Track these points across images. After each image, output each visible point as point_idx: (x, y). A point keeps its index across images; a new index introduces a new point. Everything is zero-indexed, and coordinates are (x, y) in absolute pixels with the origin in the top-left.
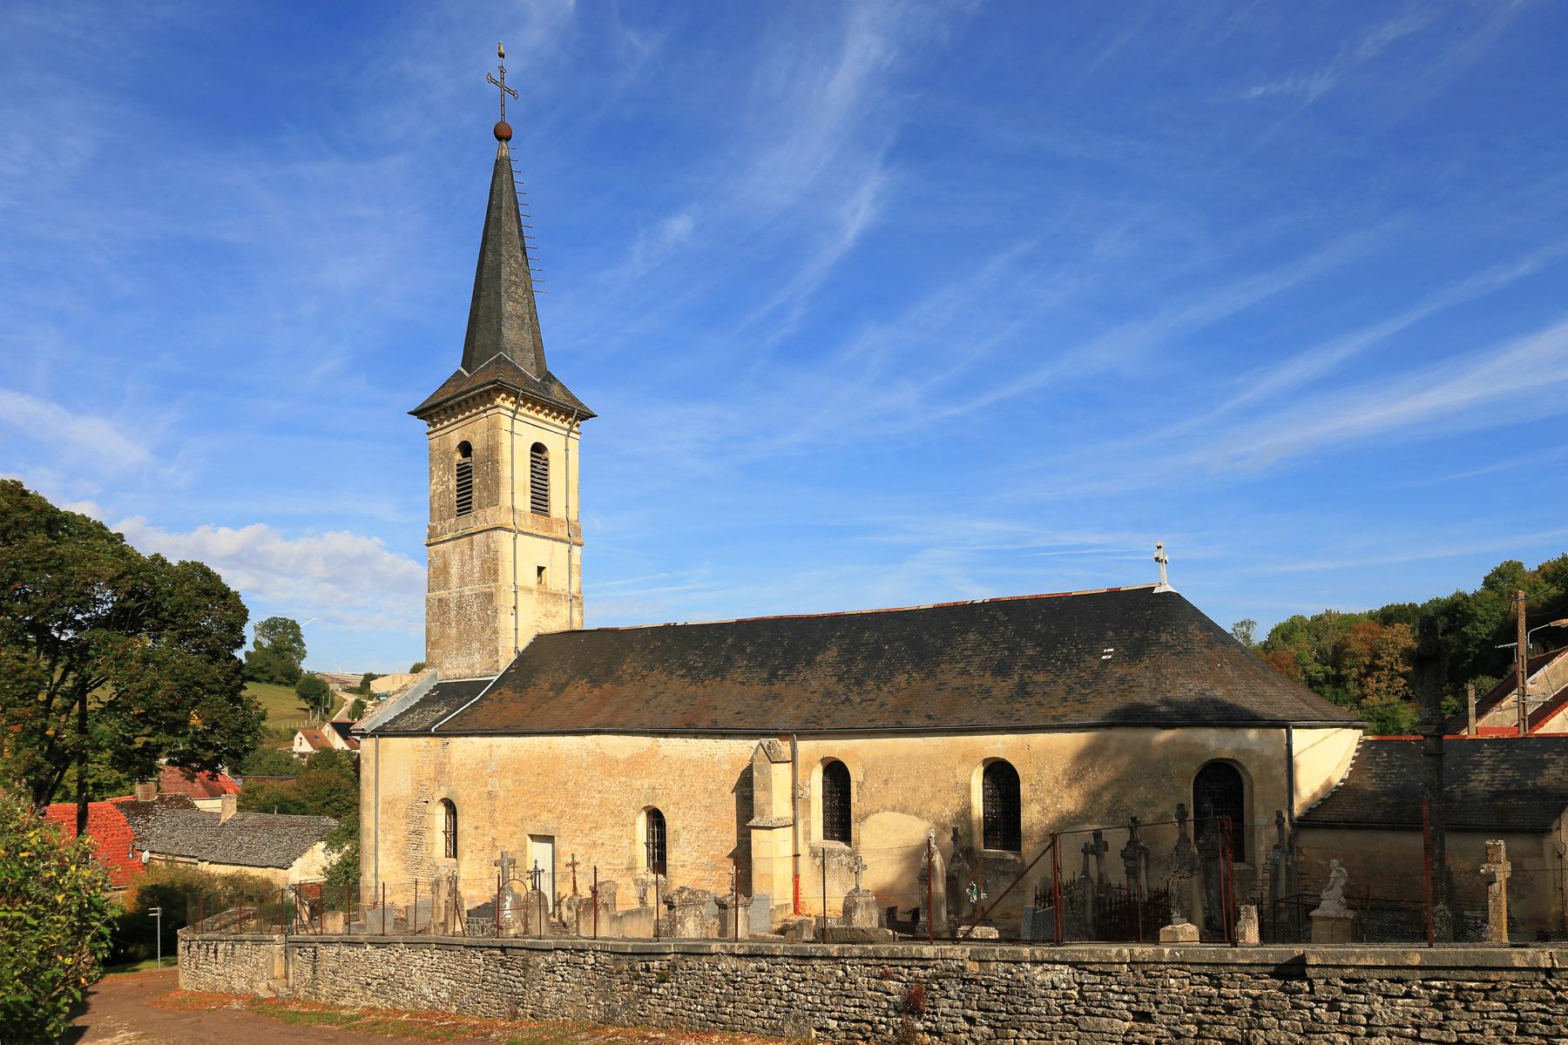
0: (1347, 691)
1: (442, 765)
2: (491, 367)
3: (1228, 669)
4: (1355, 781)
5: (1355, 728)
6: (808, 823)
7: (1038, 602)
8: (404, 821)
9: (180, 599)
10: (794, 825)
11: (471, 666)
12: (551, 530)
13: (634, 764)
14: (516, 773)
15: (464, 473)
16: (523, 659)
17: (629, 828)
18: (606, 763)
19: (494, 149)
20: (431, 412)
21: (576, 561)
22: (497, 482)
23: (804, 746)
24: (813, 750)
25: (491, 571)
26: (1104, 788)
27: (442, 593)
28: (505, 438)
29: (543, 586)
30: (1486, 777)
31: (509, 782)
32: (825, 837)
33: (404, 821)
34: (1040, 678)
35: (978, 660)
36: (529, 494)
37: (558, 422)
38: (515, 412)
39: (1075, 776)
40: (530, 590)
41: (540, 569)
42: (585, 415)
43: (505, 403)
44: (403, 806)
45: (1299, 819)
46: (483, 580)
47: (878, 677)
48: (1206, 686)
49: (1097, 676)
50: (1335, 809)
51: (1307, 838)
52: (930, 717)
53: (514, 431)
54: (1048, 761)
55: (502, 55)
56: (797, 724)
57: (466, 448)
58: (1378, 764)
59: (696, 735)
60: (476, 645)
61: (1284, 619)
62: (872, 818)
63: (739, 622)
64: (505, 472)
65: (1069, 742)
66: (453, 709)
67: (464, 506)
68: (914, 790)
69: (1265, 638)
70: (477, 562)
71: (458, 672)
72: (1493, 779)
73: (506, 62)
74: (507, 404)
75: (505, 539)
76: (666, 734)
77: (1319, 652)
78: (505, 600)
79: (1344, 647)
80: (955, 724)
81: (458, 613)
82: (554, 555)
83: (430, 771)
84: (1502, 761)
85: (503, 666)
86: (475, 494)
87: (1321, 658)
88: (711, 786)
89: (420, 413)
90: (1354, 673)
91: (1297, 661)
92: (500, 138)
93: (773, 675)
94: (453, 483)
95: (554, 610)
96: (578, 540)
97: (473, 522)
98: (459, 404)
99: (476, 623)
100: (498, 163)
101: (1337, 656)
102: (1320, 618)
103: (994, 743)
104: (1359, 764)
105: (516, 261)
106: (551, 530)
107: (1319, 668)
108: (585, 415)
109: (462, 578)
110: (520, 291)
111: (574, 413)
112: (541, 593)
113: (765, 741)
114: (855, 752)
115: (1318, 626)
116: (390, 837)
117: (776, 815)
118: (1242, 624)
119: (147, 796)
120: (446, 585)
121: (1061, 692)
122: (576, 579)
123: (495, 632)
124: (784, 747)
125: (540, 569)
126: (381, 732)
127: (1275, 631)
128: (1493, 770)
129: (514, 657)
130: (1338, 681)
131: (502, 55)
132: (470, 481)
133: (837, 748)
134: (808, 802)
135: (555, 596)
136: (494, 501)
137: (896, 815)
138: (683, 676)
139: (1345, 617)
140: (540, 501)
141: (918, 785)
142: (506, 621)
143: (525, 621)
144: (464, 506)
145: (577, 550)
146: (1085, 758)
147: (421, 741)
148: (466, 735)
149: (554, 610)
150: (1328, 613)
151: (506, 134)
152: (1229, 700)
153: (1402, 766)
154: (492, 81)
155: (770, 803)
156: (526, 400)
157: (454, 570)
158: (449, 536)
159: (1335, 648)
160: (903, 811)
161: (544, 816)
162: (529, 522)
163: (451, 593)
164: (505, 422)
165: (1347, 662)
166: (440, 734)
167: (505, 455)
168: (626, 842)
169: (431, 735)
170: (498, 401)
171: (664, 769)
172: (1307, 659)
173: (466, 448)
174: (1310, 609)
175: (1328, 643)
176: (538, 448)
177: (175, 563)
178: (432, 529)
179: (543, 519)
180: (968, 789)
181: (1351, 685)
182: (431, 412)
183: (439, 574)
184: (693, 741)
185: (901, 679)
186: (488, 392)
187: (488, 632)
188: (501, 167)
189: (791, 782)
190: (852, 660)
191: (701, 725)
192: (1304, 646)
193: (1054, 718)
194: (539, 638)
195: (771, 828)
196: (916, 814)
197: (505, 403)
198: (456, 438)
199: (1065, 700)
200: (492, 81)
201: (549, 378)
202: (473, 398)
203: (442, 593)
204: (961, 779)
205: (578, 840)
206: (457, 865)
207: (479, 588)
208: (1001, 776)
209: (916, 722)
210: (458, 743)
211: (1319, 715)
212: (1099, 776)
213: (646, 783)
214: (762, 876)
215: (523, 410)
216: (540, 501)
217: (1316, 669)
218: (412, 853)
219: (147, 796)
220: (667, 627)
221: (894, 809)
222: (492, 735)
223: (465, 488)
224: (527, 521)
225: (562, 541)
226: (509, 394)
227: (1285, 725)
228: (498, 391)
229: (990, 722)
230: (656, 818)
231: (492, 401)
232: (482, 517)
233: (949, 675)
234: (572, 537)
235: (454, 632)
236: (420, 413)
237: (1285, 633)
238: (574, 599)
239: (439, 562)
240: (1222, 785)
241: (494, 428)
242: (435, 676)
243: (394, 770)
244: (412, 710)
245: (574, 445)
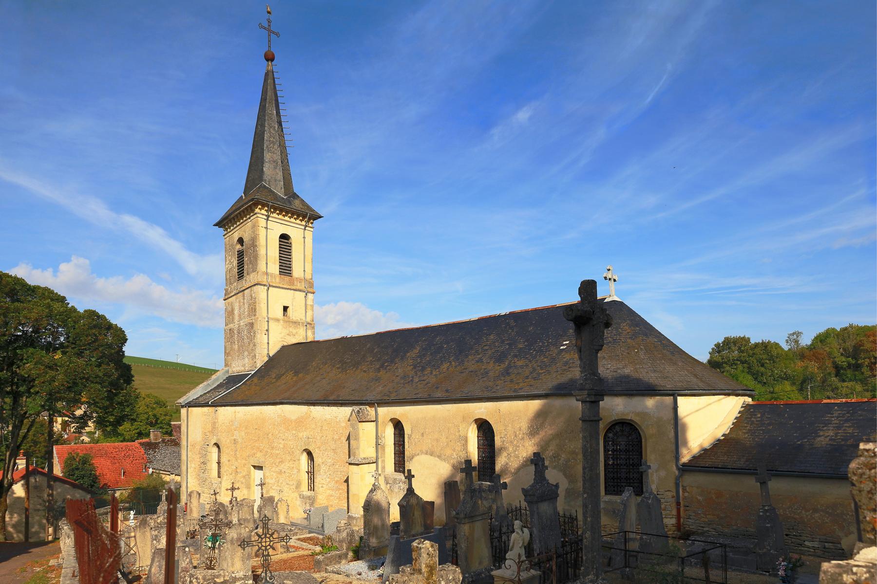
0: (863, 373)
1: (215, 423)
2: (265, 192)
3: (642, 355)
4: (734, 436)
5: (737, 395)
6: (383, 461)
7: (536, 311)
8: (198, 456)
9: (78, 331)
10: (376, 462)
11: (244, 366)
12: (293, 284)
13: (300, 422)
14: (246, 428)
15: (241, 255)
16: (272, 362)
17: (297, 462)
18: (286, 421)
19: (264, 66)
20: (226, 222)
21: (309, 302)
22: (256, 257)
23: (382, 410)
24: (386, 412)
25: (253, 310)
26: (550, 440)
27: (231, 326)
28: (262, 232)
29: (284, 317)
30: (831, 433)
31: (243, 434)
32: (395, 471)
33: (198, 456)
34: (520, 363)
35: (490, 352)
36: (278, 267)
37: (298, 221)
38: (268, 216)
39: (533, 432)
40: (278, 320)
41: (285, 309)
42: (315, 217)
43: (261, 213)
44: (198, 447)
45: (684, 465)
46: (249, 315)
47: (434, 366)
48: (620, 366)
49: (553, 360)
50: (718, 458)
51: (689, 480)
52: (447, 391)
53: (267, 228)
54: (516, 422)
55: (269, 13)
56: (379, 397)
57: (241, 241)
58: (753, 422)
59: (329, 404)
60: (246, 353)
61: (822, 329)
62: (415, 459)
63: (378, 334)
64: (262, 251)
65: (527, 408)
66: (239, 391)
67: (241, 275)
68: (437, 440)
69: (809, 343)
70: (246, 306)
71: (238, 369)
72: (836, 435)
73: (271, 17)
74: (263, 212)
75: (261, 291)
76: (314, 404)
77: (844, 350)
78: (261, 326)
79: (860, 346)
80: (458, 396)
81: (239, 337)
82: (296, 300)
83: (209, 427)
84: (846, 421)
85: (259, 366)
86: (246, 267)
87: (846, 353)
88: (336, 437)
89: (219, 224)
90: (867, 362)
91: (829, 354)
92: (267, 60)
93: (382, 366)
94: (235, 263)
95: (294, 331)
96: (311, 290)
97: (245, 283)
98: (236, 216)
99: (246, 341)
100: (267, 75)
101: (856, 352)
102: (846, 329)
103: (480, 408)
104: (738, 423)
105: (274, 129)
106: (293, 284)
107: (844, 359)
108: (315, 217)
109: (240, 315)
110: (276, 147)
111: (309, 216)
112: (285, 321)
113: (356, 408)
114: (407, 413)
115: (845, 333)
116: (193, 465)
117: (362, 456)
118: (793, 334)
119: (156, 439)
120: (233, 321)
121: (527, 373)
122: (309, 313)
123: (255, 345)
124: (371, 411)
125: (285, 309)
126: (190, 405)
127: (816, 338)
128: (839, 428)
129: (266, 359)
130: (857, 367)
131: (269, 13)
132: (243, 260)
133: (397, 412)
134: (383, 447)
135: (296, 323)
136: (254, 270)
137: (428, 457)
138: (338, 368)
139: (861, 328)
140: (285, 267)
141: (440, 438)
142: (261, 338)
143: (274, 338)
144: (241, 275)
145: (310, 296)
146: (541, 416)
147: (206, 409)
148: (225, 406)
149: (294, 331)
150: (851, 326)
151: (271, 57)
152: (635, 375)
153: (769, 424)
154: (277, 34)
155: (358, 448)
156: (275, 209)
157: (236, 312)
158: (235, 292)
159: (854, 346)
160: (432, 454)
161: (259, 455)
162: (278, 280)
163: (234, 326)
164: (262, 222)
165: (862, 355)
166: (215, 405)
167: (262, 241)
168: (295, 471)
169: (210, 406)
170: (257, 210)
171: (313, 426)
172: (836, 353)
173: (241, 241)
174: (839, 323)
175: (850, 344)
176: (284, 237)
177: (82, 311)
178: (226, 290)
179: (287, 278)
180: (466, 440)
181: (865, 369)
182: (226, 222)
183: (230, 314)
184: (327, 408)
185: (445, 366)
186: (250, 206)
187: (251, 345)
188: (269, 76)
189: (373, 433)
190: (424, 355)
191: (331, 398)
192: (835, 347)
193: (515, 391)
194: (283, 348)
195: (358, 465)
196: (439, 457)
197: (261, 213)
198: (236, 236)
199: (527, 377)
200: (277, 34)
201: (295, 196)
202: (243, 211)
203: (231, 326)
204: (462, 433)
205: (273, 469)
206: (221, 483)
207: (247, 320)
208: (485, 428)
209: (438, 394)
210: (222, 410)
211: (701, 385)
212: (548, 431)
213: (305, 434)
214: (354, 495)
215: (275, 215)
216: (285, 267)
217: (842, 360)
218: (202, 475)
219: (156, 439)
220: (343, 338)
221: (426, 454)
222: (235, 405)
223: (241, 264)
224: (277, 280)
225: (300, 291)
226: (263, 206)
227: (674, 394)
228: (256, 205)
229: (480, 394)
230: (310, 454)
231: (253, 211)
232: (251, 279)
233: (471, 364)
234: (309, 288)
235: (236, 347)
236: (219, 224)
237: (822, 339)
238: (310, 325)
239: (229, 309)
240: (627, 439)
241: (255, 226)
242: (228, 372)
243: (195, 424)
244: (208, 392)
245: (309, 234)
